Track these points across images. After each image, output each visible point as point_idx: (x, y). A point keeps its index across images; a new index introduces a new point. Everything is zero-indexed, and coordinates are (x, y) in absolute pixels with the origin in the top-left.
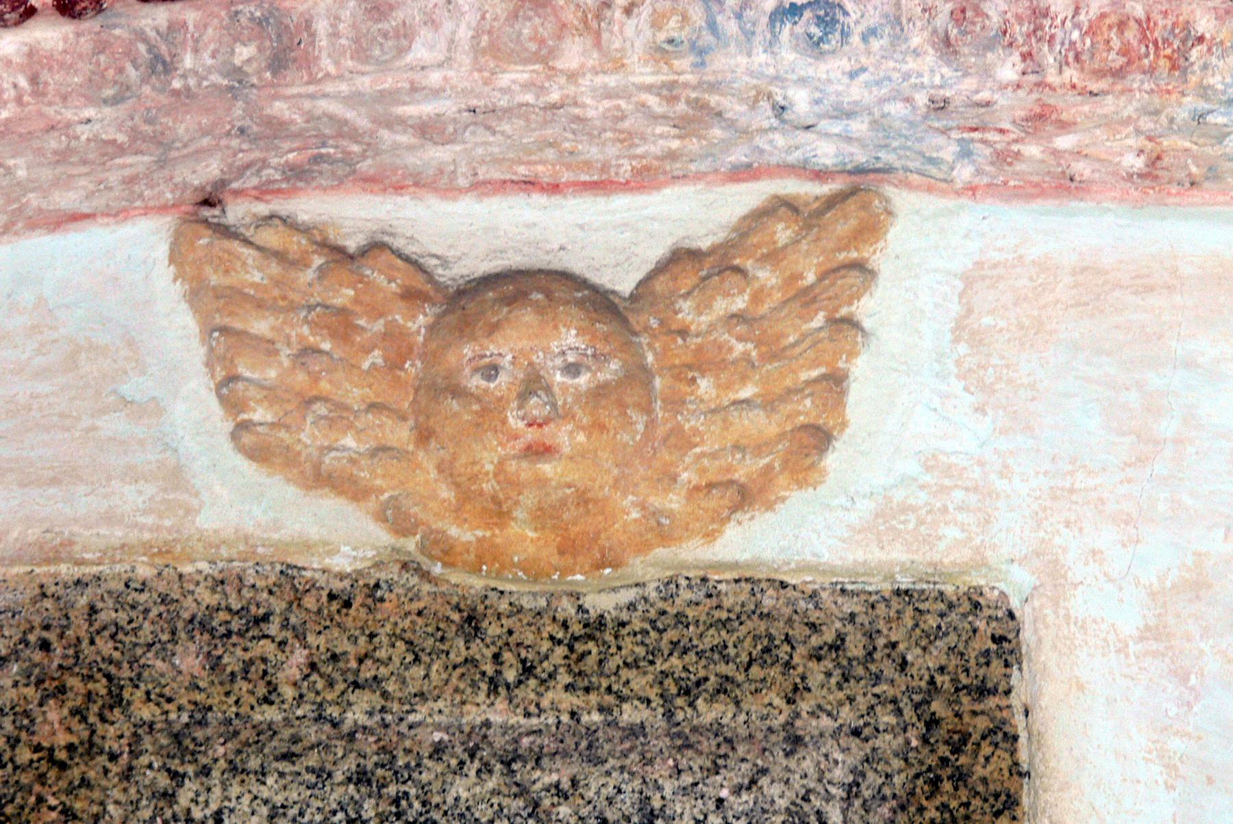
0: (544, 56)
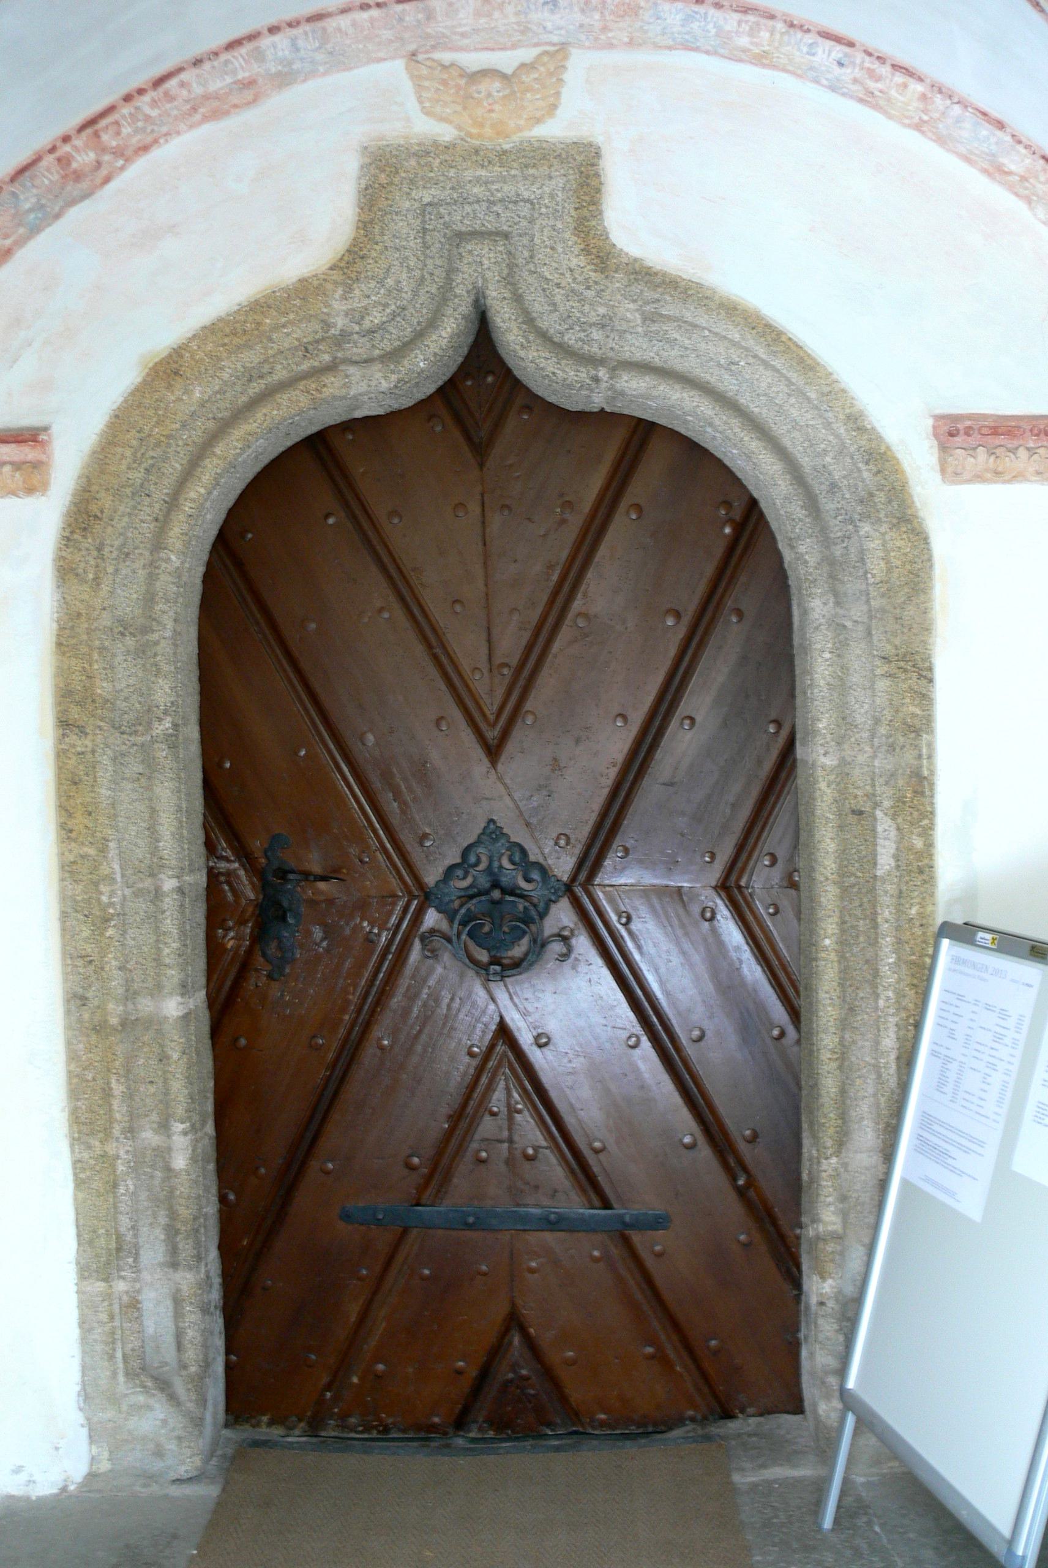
0: (489, 15)
